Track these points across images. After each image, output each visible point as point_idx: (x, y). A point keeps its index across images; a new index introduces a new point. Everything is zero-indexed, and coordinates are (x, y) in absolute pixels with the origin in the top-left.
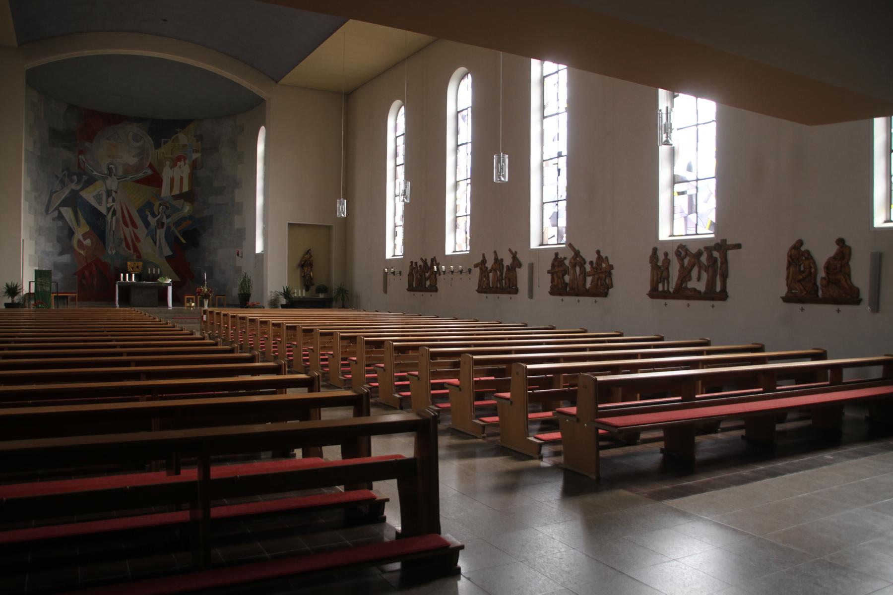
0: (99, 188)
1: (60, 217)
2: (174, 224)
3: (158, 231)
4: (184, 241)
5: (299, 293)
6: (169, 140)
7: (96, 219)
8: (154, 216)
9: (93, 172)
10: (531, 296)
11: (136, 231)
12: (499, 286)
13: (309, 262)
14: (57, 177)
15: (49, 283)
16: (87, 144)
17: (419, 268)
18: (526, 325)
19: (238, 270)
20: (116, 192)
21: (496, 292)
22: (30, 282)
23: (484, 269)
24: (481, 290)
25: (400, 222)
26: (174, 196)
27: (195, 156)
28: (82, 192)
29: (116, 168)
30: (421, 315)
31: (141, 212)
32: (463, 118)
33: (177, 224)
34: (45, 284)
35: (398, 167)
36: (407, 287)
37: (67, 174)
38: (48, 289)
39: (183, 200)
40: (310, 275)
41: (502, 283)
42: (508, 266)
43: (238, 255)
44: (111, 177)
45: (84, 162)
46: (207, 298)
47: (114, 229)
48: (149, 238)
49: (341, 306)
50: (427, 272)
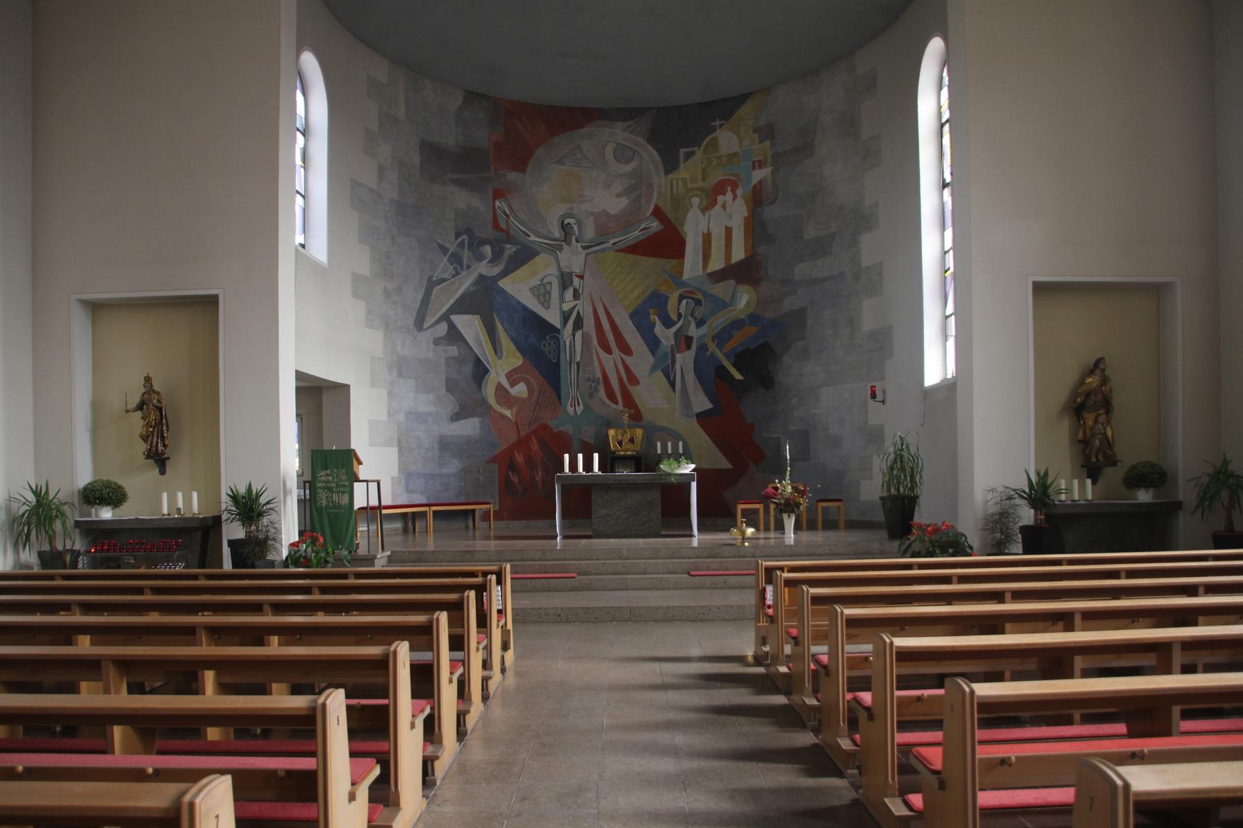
0: (543, 268)
1: (454, 336)
2: (713, 339)
4: (738, 376)
8: (668, 323)
9: (529, 236)
11: (628, 360)
14: (444, 250)
16: (512, 176)
19: (875, 436)
20: (581, 277)
26: (710, 275)
27: (758, 175)
28: (504, 280)
29: (579, 223)
31: (639, 317)
33: (721, 337)
34: (338, 486)
37: (466, 242)
39: (732, 282)
40: (1105, 434)
43: (874, 396)
44: (569, 244)
46: (793, 511)
47: (578, 359)
48: (659, 373)
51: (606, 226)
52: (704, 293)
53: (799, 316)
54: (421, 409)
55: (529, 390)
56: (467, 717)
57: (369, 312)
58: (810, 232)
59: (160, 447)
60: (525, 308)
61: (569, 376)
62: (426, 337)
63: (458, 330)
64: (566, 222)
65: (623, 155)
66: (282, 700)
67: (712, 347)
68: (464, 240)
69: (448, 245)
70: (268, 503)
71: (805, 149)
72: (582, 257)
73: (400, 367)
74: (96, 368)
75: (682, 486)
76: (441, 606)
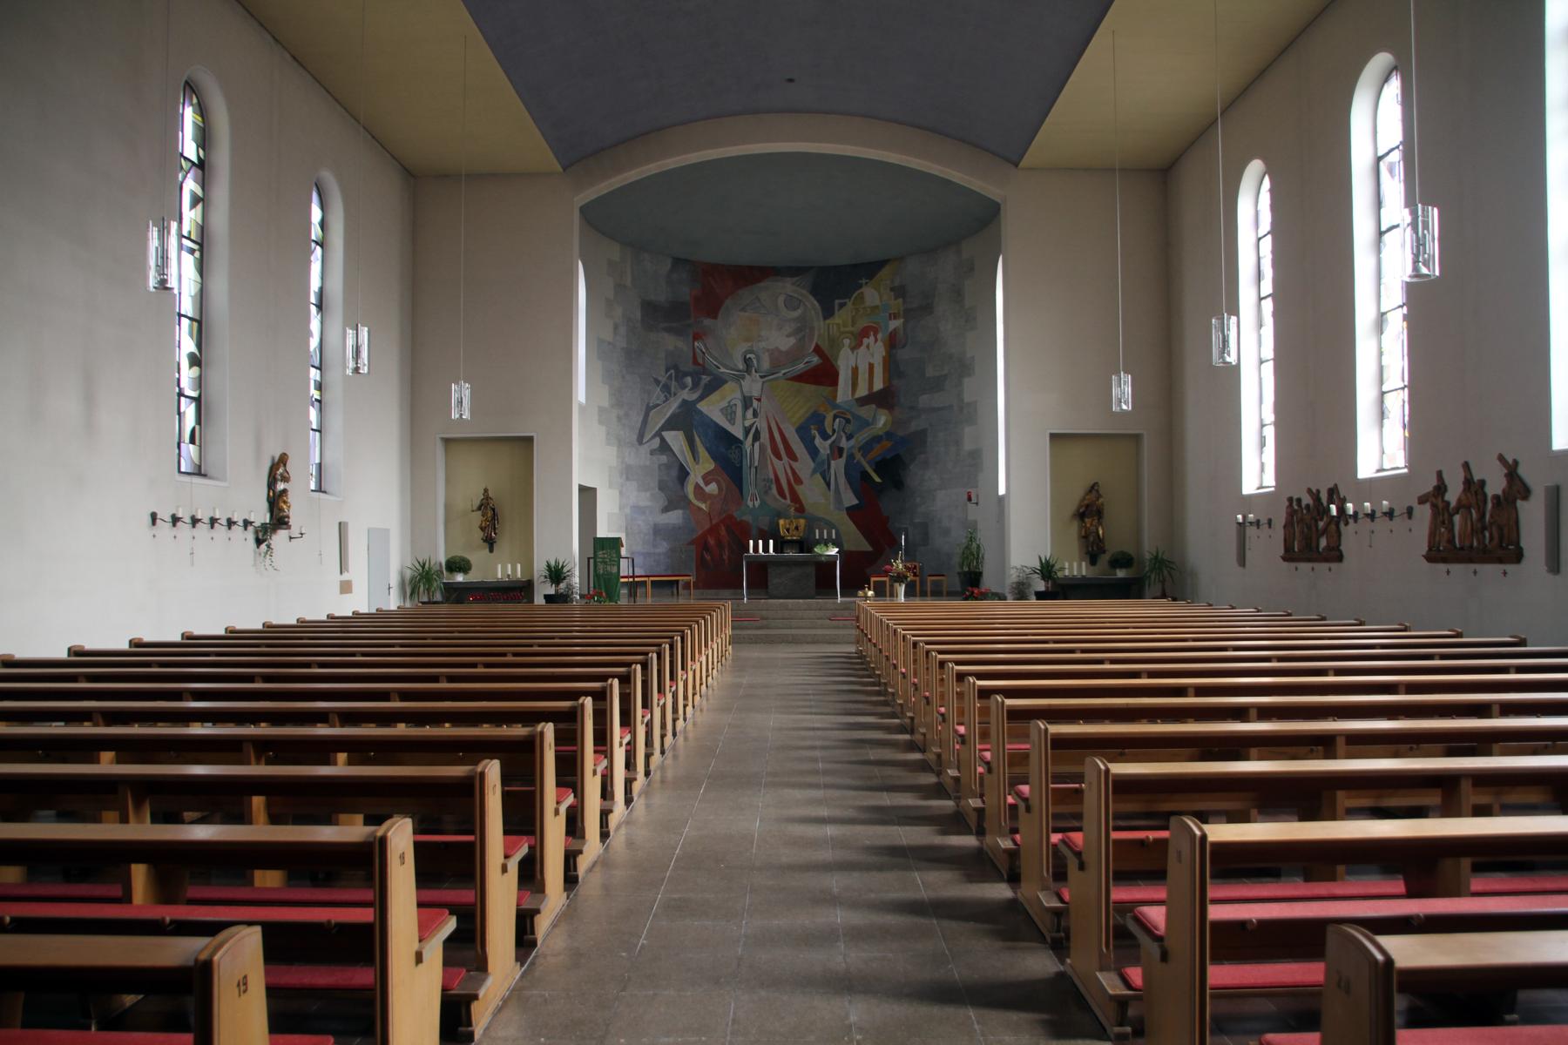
0: (730, 394)
1: (665, 447)
3: (833, 463)
4: (878, 480)
5: (1074, 567)
6: (847, 300)
7: (725, 448)
8: (825, 437)
10: (1554, 565)
11: (794, 465)
12: (1475, 544)
13: (1095, 509)
14: (657, 382)
15: (616, 559)
16: (707, 322)
17: (1305, 511)
18: (1522, 643)
20: (759, 400)
21: (1471, 561)
22: (589, 559)
23: (1440, 505)
24: (1433, 556)
25: (1269, 417)
26: (857, 400)
27: (894, 324)
30: (1290, 615)
31: (803, 431)
32: (1391, 171)
33: (866, 448)
35: (1263, 302)
36: (1282, 551)
37: (673, 375)
38: (615, 570)
39: (874, 406)
41: (1484, 536)
42: (1496, 497)
45: (703, 353)
46: (903, 582)
47: (756, 464)
48: (818, 476)
49: (1159, 594)
50: (1321, 520)
51: (778, 360)
52: (853, 414)
53: (921, 436)
54: (642, 504)
55: (719, 489)
56: (537, 918)
57: (608, 434)
58: (930, 372)
59: (493, 535)
60: (716, 425)
61: (749, 477)
62: (645, 449)
63: (667, 443)
64: (748, 357)
65: (792, 303)
66: (350, 831)
67: (858, 456)
68: (671, 374)
69: (660, 379)
70: (568, 571)
71: (927, 309)
72: (760, 384)
73: (628, 472)
74: (448, 481)
75: (831, 562)
76: (586, 693)
